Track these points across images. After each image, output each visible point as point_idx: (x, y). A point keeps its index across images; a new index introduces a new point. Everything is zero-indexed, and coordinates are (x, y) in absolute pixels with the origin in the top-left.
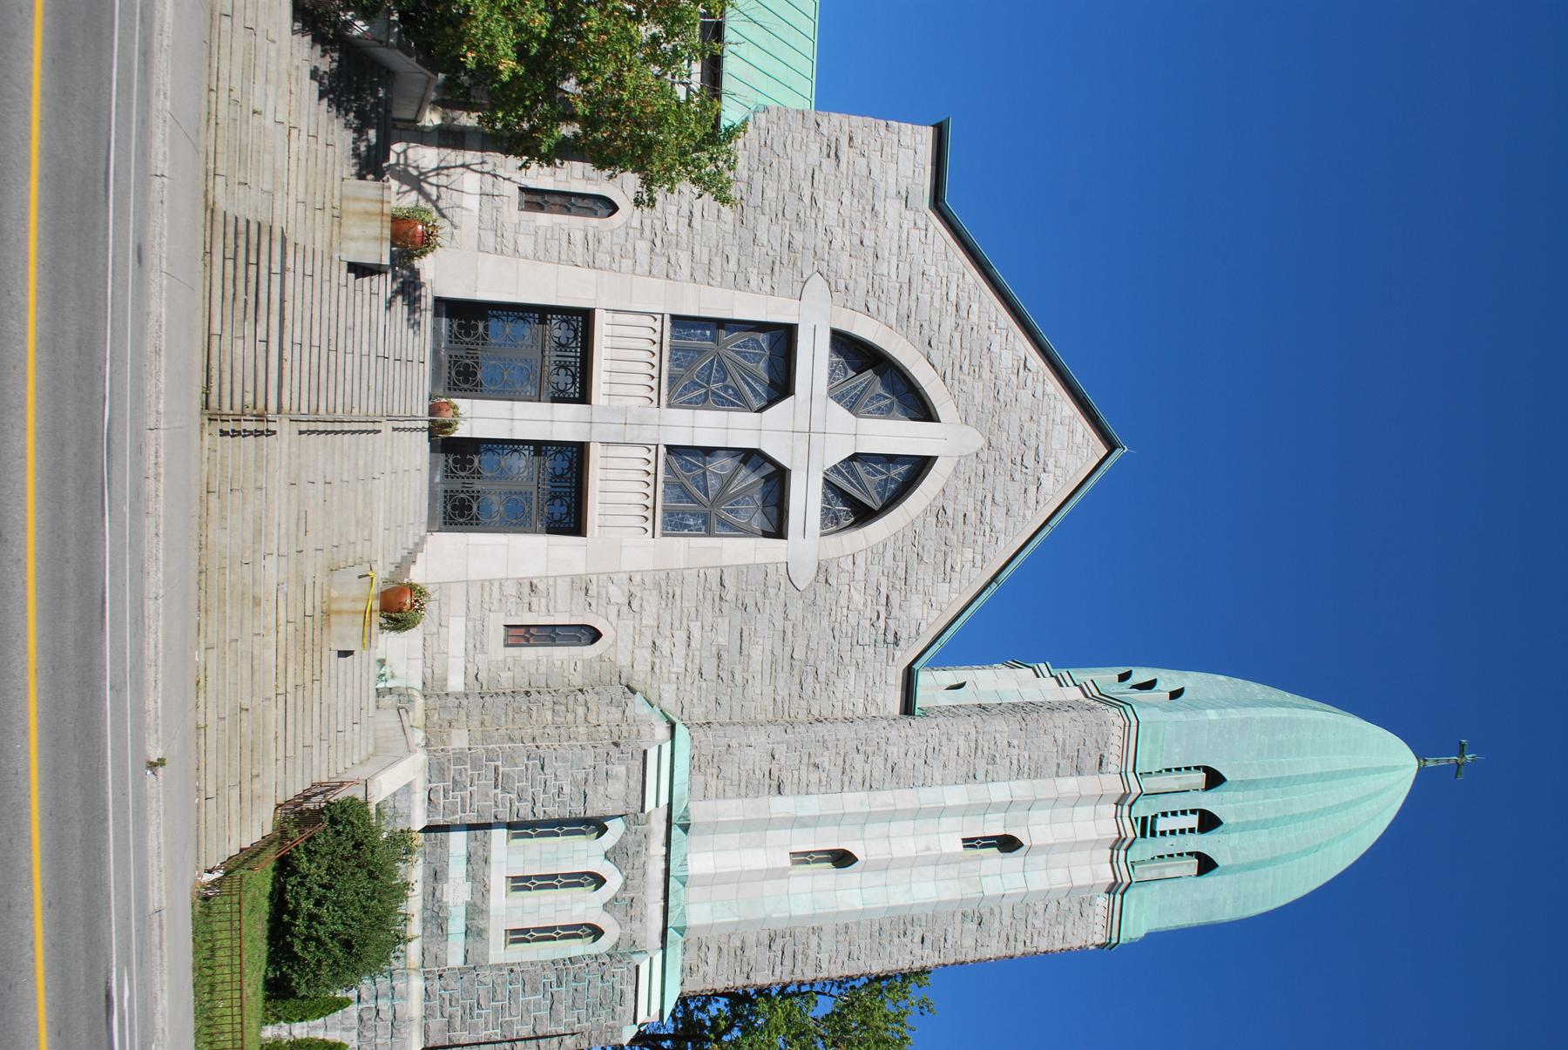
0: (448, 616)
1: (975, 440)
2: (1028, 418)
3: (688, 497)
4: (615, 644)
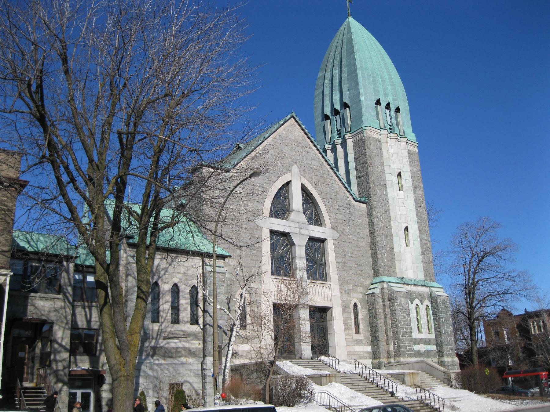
0: (355, 352)
1: (295, 169)
2: (287, 147)
3: (315, 272)
4: (357, 298)
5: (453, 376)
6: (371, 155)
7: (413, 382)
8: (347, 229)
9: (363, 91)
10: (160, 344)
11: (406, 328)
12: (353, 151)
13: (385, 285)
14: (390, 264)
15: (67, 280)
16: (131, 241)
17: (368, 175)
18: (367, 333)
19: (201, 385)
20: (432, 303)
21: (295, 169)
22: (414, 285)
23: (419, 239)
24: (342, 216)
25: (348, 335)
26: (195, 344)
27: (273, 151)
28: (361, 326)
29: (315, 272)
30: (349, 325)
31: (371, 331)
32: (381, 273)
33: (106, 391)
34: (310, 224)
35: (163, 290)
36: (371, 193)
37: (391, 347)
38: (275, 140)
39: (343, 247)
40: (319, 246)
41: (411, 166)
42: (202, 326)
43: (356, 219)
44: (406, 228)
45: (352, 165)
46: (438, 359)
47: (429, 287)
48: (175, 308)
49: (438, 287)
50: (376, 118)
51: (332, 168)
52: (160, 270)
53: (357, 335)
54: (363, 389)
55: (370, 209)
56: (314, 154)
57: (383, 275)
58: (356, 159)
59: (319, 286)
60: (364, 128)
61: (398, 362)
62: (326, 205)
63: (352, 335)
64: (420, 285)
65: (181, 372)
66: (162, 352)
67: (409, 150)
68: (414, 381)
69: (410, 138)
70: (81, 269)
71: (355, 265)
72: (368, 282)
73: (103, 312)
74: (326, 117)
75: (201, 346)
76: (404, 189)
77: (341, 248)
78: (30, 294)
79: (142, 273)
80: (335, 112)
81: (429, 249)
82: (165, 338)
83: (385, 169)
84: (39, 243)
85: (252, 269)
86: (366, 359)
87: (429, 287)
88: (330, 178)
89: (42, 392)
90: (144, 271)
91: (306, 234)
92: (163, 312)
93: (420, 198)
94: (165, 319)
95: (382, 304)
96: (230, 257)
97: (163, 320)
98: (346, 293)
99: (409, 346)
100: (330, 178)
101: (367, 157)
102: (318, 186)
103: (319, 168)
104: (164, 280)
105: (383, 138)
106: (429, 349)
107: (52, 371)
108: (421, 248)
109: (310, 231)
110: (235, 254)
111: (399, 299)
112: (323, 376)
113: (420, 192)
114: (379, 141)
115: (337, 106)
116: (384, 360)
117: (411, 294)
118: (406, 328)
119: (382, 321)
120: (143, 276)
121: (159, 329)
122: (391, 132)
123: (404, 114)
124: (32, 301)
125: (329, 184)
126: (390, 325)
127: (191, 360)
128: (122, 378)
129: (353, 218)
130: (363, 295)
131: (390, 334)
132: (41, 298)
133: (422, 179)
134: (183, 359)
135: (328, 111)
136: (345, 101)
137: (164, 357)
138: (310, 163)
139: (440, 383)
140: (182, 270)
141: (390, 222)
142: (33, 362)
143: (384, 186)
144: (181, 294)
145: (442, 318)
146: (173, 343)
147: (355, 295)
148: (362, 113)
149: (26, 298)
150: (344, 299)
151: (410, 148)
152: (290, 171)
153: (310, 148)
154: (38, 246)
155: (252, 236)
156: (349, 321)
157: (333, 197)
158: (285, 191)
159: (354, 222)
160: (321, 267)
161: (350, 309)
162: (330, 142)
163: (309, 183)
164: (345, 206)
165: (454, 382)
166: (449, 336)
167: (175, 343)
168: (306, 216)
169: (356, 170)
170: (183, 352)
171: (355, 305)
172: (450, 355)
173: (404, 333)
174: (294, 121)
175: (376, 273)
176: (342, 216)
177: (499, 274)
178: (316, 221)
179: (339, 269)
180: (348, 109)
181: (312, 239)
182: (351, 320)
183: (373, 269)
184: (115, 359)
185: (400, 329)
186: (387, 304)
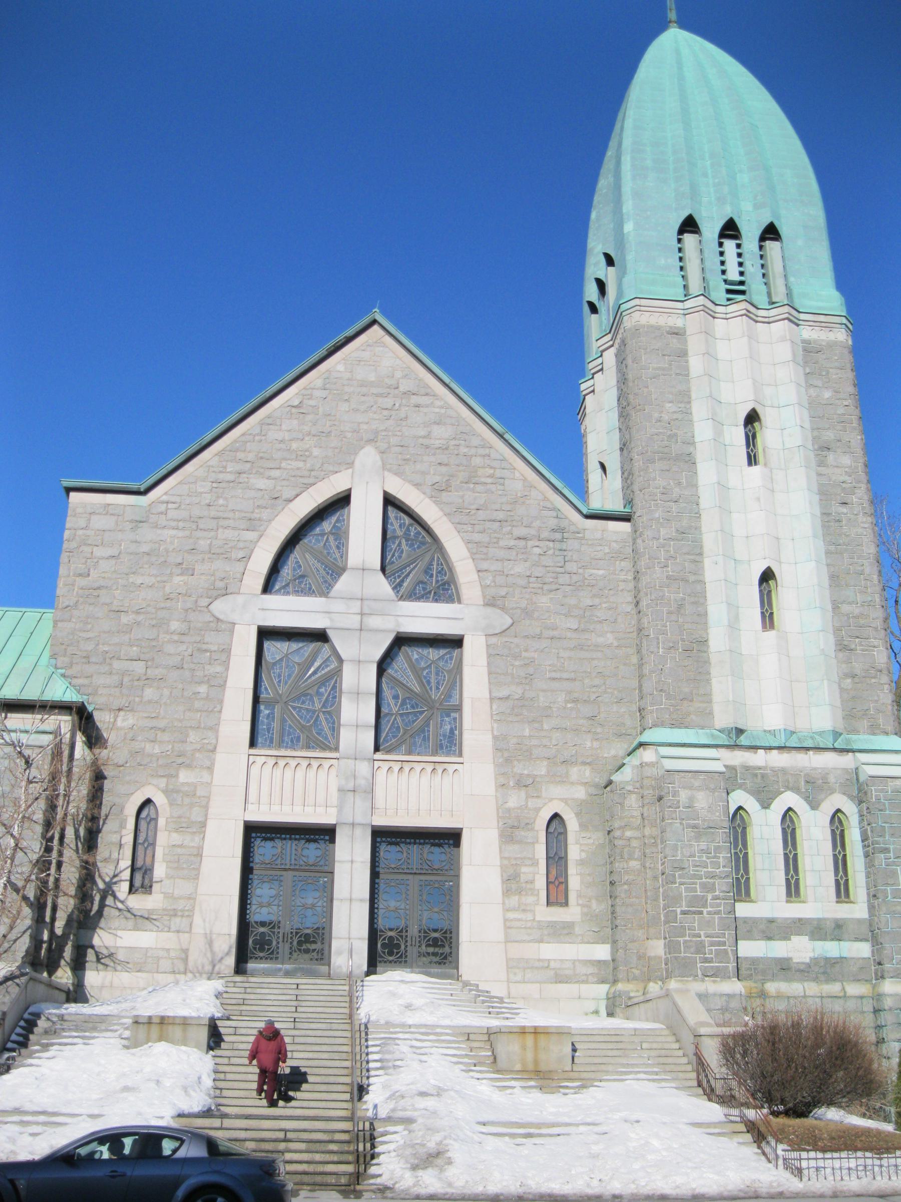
0: (539, 960)
1: (368, 457)
4: (565, 801)
7: (536, 1062)
8: (544, 601)
11: (704, 886)
18: (594, 905)
21: (368, 457)
25: (513, 909)
27: (295, 422)
28: (574, 882)
30: (523, 878)
34: (401, 598)
39: (524, 654)
46: (874, 987)
56: (442, 407)
57: (655, 725)
62: (468, 542)
63: (533, 912)
64: (808, 749)
67: (804, 341)
71: (567, 702)
77: (516, 657)
83: (694, 410)
85: (187, 736)
86: (586, 982)
87: (853, 751)
98: (521, 784)
99: (712, 944)
100: (496, 464)
102: (444, 494)
103: (457, 442)
105: (693, 324)
108: (837, 630)
109: (400, 619)
111: (683, 795)
118: (704, 886)
125: (489, 480)
129: (572, 567)
130: (593, 790)
145: (886, 850)
147: (557, 791)
153: (427, 394)
155: (199, 649)
156: (524, 869)
157: (501, 515)
159: (575, 578)
160: (448, 716)
163: (412, 488)
164: (545, 534)
174: (381, 332)
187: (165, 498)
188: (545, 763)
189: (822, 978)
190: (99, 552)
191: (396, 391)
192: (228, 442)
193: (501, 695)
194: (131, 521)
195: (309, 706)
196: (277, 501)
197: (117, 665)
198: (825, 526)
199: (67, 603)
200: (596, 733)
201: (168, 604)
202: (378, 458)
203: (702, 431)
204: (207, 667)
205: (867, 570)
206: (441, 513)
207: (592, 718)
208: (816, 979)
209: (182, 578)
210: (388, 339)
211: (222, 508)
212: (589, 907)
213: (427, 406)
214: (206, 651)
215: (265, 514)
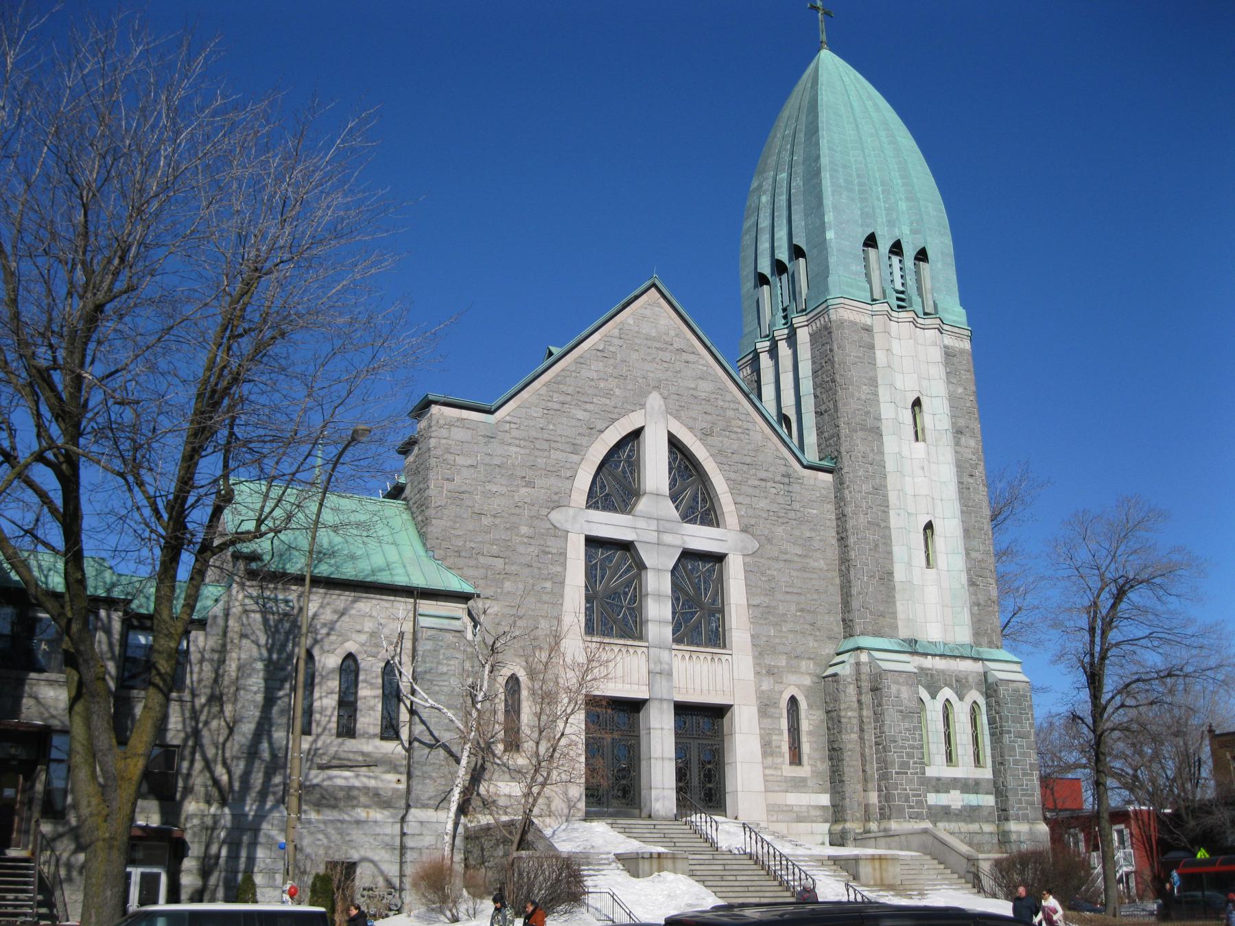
1: (655, 401)
2: (637, 353)
4: (798, 686)
5: (985, 867)
6: (844, 363)
7: (882, 879)
8: (779, 530)
9: (832, 218)
10: (311, 780)
11: (908, 754)
12: (808, 355)
13: (864, 657)
14: (882, 609)
15: (105, 647)
16: (254, 565)
17: (836, 409)
18: (819, 763)
19: (397, 867)
20: (988, 696)
21: (655, 401)
22: (941, 656)
23: (961, 550)
24: (768, 501)
26: (389, 782)
27: (601, 364)
28: (806, 748)
29: (697, 627)
31: (831, 759)
32: (858, 629)
33: (189, 871)
35: (323, 668)
36: (843, 450)
37: (873, 798)
38: (607, 340)
40: (711, 571)
41: (949, 382)
42: (407, 745)
43: (804, 507)
44: (929, 526)
45: (807, 386)
46: (998, 826)
47: (982, 660)
48: (348, 705)
49: (1007, 662)
50: (863, 278)
51: (746, 395)
52: (318, 627)
53: (798, 768)
54: (743, 889)
55: (840, 485)
56: (703, 365)
57: (862, 634)
58: (815, 372)
59: (723, 660)
60: (830, 302)
61: (885, 830)
62: (727, 480)
63: (781, 769)
64: (956, 657)
65: (354, 837)
66: (316, 796)
67: (945, 347)
68: (885, 875)
69: (948, 318)
70: (134, 622)
71: (797, 611)
72: (829, 649)
73: (73, 713)
74: (762, 280)
75: (403, 786)
76: (928, 437)
77: (763, 574)
78: (27, 675)
79: (161, 636)
80: (779, 267)
81: (989, 574)
82: (322, 767)
84: (51, 573)
85: (539, 623)
87: (982, 660)
88: (743, 417)
89: (27, 868)
90: (165, 631)
91: (673, 543)
92: (321, 713)
93: (971, 456)
94: (325, 729)
95: (855, 699)
96: (478, 596)
97: (320, 730)
98: (771, 672)
99: (914, 796)
100: (743, 417)
101: (837, 366)
102: (709, 438)
103: (715, 396)
104: (326, 648)
105: (878, 323)
106: (974, 803)
107: (66, 828)
108: (969, 570)
109: (685, 538)
110: (499, 590)
111: (894, 688)
112: (643, 858)
113: (971, 443)
114: (868, 329)
115: (783, 255)
116: (853, 826)
117: (932, 675)
118: (908, 754)
119: (854, 736)
120: (162, 642)
121: (310, 749)
122: (899, 307)
123: (939, 265)
124: (31, 689)
125: (739, 430)
126: (871, 747)
127: (377, 815)
128: (100, 844)
129: (796, 506)
131: (873, 769)
132: (50, 683)
133: (979, 411)
134: (361, 813)
135: (765, 268)
136: (795, 242)
137: (319, 805)
138: (692, 386)
139: (964, 886)
140: (368, 626)
141: (886, 513)
142: (30, 808)
143: (876, 433)
144: (361, 677)
145: (1009, 732)
146: (342, 778)
147: (792, 678)
148: (827, 267)
149: (21, 682)
150: (765, 687)
151: (949, 341)
152: (643, 406)
154: (50, 579)
156: (774, 737)
157: (748, 460)
158: (630, 451)
161: (778, 711)
162: (768, 336)
164: (778, 478)
165: (987, 882)
166: (1024, 774)
167: (346, 778)
168: (677, 508)
169: (816, 396)
170: (363, 799)
171: (793, 700)
172: (1025, 819)
173: (905, 765)
174: (658, 295)
175: (849, 629)
176: (768, 501)
177: (1159, 630)
178: (707, 513)
179: (754, 621)
180: (802, 260)
181: (687, 555)
182: (781, 734)
183: (844, 620)
184: (89, 805)
185: (893, 756)
186: (867, 698)
187: (508, 418)
188: (785, 657)
189: (968, 819)
190: (460, 460)
191: (671, 348)
192: (553, 375)
193: (755, 603)
194: (484, 436)
195: (614, 599)
196: (594, 432)
197: (482, 560)
198: (961, 492)
199: (439, 504)
200: (815, 636)
201: (517, 511)
202: (662, 402)
203: (886, 411)
204: (550, 567)
205: (986, 527)
206: (708, 454)
207: (812, 624)
208: (964, 821)
209: (527, 490)
210: (662, 301)
211: (552, 433)
212: (815, 766)
213: (694, 363)
214: (549, 553)
215: (584, 441)
